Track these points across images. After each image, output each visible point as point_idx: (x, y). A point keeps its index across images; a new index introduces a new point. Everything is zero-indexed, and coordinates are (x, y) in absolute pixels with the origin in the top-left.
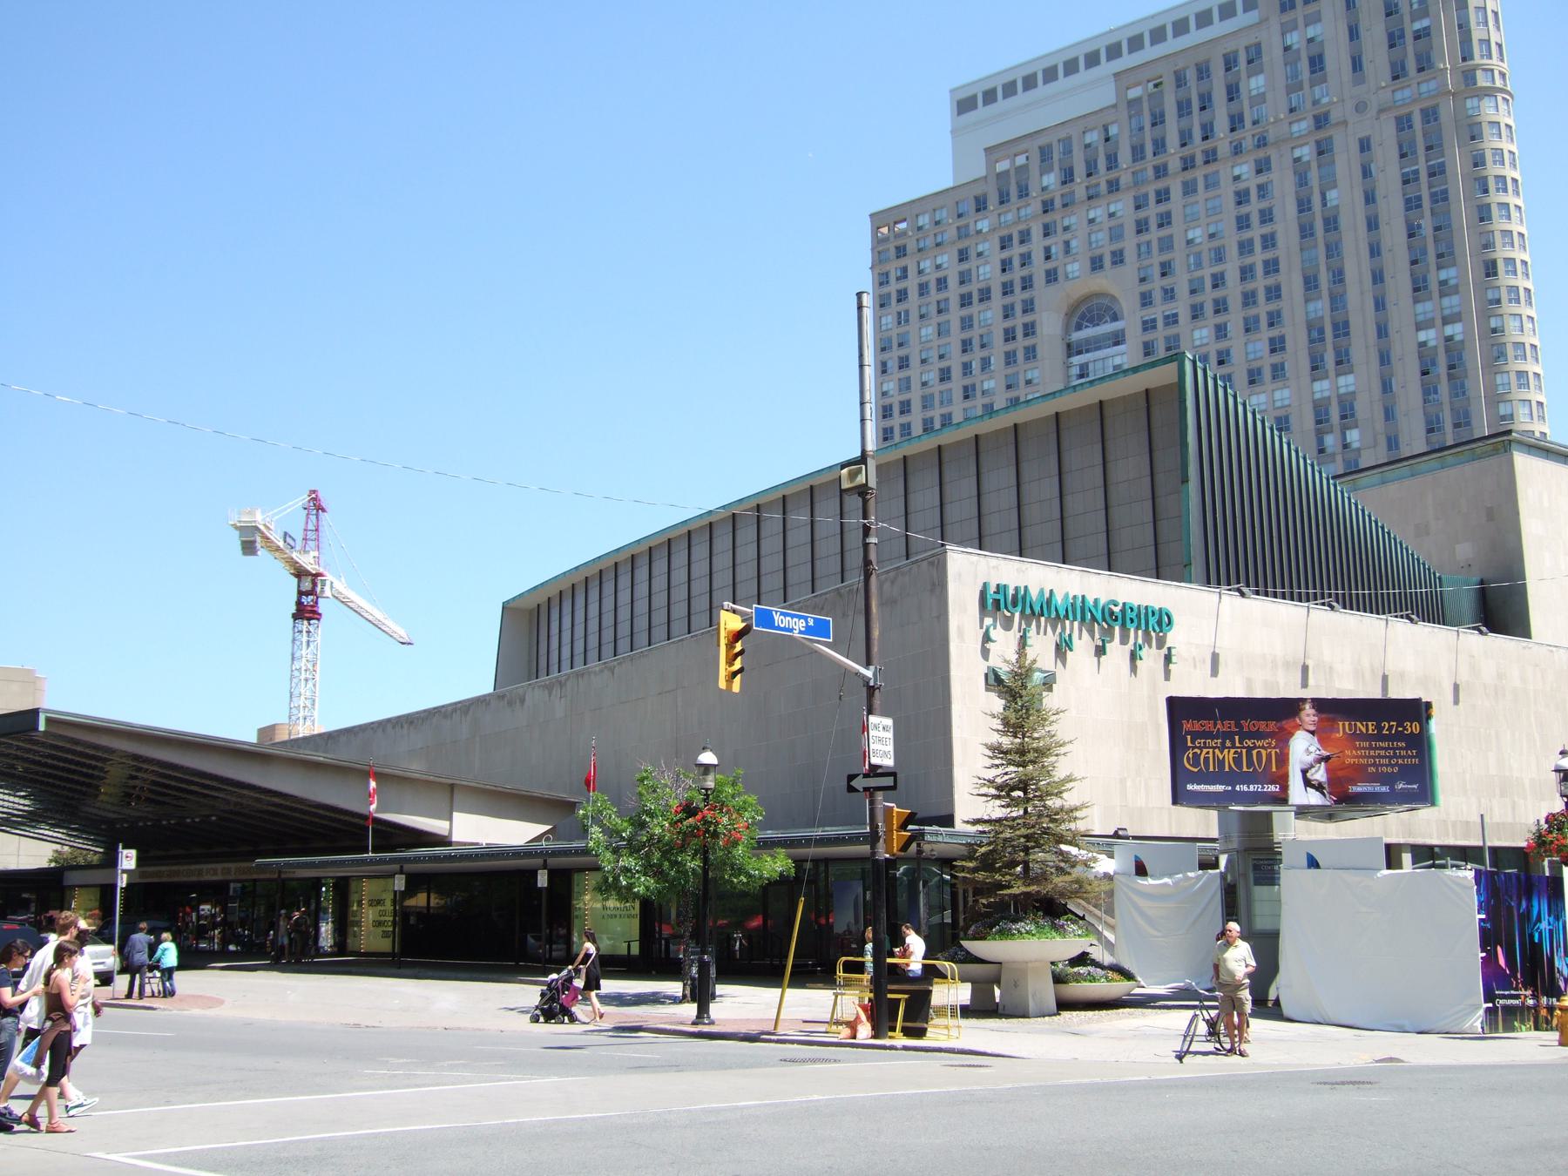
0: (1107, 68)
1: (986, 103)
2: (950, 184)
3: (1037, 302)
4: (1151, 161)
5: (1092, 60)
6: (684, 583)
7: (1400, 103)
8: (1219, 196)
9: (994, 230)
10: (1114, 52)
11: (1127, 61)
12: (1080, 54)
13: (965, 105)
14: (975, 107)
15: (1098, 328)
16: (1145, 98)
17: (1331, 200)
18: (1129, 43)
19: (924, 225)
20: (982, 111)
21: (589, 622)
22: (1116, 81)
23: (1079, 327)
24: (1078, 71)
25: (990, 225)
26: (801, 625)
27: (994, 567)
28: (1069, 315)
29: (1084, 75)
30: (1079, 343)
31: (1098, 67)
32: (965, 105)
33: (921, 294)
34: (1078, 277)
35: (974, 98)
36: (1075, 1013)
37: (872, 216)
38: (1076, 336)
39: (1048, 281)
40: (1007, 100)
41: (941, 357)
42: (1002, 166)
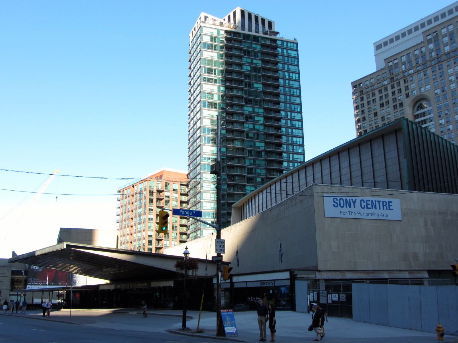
0: (421, 31)
1: (390, 43)
2: (375, 70)
3: (403, 104)
4: (407, 70)
5: (416, 29)
6: (295, 188)
7: (380, 87)
8: (428, 77)
9: (416, 72)
10: (423, 25)
11: (427, 27)
12: (388, 40)
13: (378, 47)
14: (381, 47)
15: (423, 110)
16: (433, 38)
17: (422, 90)
18: (388, 44)
19: (368, 84)
20: (384, 49)
21: (277, 197)
22: (423, 34)
23: (418, 110)
24: (393, 42)
25: (387, 82)
26: (190, 213)
27: (330, 189)
28: (414, 107)
29: (414, 34)
30: (418, 115)
31: (381, 49)
32: (378, 47)
33: (368, 105)
34: (430, 90)
35: (381, 44)
36: (249, 272)
37: (352, 83)
38: (417, 113)
39: (407, 97)
40: (409, 35)
41: (376, 123)
42: (390, 64)
